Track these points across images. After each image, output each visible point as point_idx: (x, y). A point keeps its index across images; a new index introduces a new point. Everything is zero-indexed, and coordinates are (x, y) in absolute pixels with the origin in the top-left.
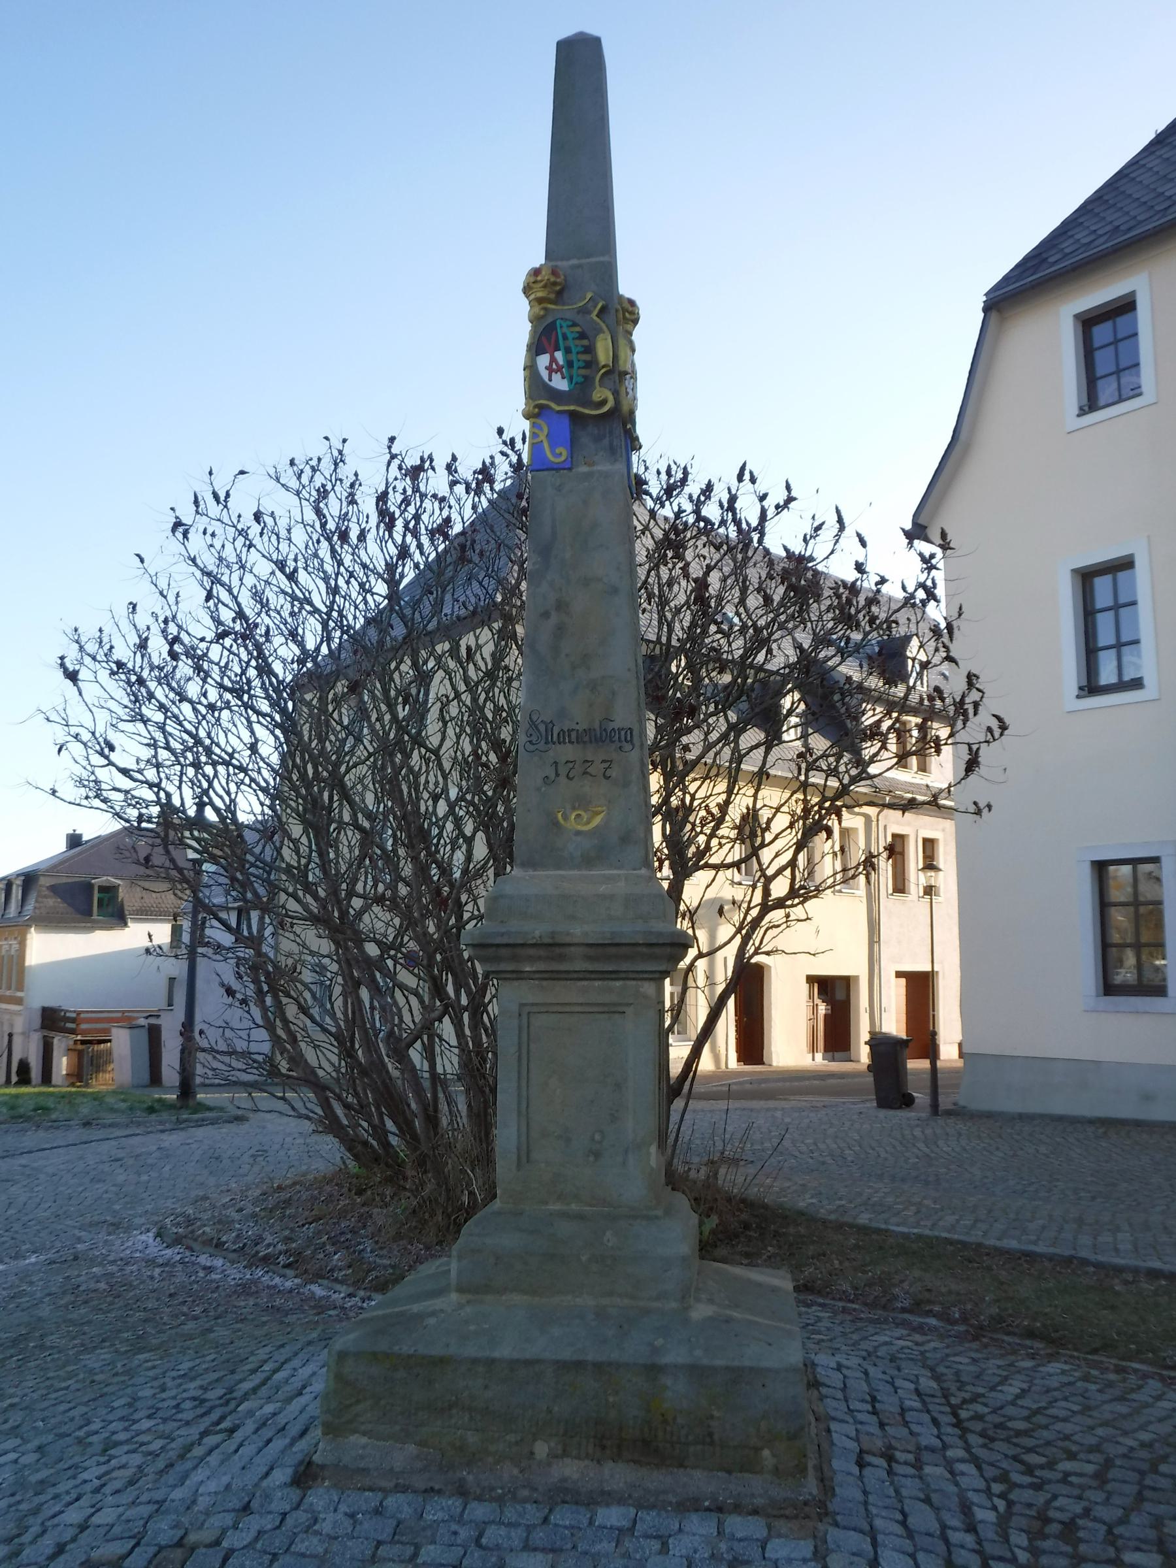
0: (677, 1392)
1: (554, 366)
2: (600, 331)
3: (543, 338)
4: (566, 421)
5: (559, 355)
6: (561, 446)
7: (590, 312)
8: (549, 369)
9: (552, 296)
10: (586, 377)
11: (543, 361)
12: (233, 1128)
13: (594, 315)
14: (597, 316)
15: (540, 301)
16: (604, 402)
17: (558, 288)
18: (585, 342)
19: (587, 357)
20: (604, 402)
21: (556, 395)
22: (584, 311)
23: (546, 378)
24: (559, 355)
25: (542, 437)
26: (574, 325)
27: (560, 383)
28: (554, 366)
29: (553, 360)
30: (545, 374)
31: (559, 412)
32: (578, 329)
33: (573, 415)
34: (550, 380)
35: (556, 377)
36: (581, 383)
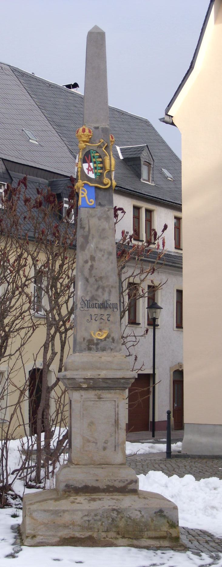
2: (106, 155)
3: (86, 157)
4: (94, 189)
5: (91, 164)
7: (102, 148)
10: (101, 173)
11: (85, 166)
13: (103, 149)
18: (101, 160)
22: (100, 147)
26: (97, 152)
27: (92, 175)
29: (89, 166)
30: (86, 171)
32: (98, 154)
35: (91, 173)
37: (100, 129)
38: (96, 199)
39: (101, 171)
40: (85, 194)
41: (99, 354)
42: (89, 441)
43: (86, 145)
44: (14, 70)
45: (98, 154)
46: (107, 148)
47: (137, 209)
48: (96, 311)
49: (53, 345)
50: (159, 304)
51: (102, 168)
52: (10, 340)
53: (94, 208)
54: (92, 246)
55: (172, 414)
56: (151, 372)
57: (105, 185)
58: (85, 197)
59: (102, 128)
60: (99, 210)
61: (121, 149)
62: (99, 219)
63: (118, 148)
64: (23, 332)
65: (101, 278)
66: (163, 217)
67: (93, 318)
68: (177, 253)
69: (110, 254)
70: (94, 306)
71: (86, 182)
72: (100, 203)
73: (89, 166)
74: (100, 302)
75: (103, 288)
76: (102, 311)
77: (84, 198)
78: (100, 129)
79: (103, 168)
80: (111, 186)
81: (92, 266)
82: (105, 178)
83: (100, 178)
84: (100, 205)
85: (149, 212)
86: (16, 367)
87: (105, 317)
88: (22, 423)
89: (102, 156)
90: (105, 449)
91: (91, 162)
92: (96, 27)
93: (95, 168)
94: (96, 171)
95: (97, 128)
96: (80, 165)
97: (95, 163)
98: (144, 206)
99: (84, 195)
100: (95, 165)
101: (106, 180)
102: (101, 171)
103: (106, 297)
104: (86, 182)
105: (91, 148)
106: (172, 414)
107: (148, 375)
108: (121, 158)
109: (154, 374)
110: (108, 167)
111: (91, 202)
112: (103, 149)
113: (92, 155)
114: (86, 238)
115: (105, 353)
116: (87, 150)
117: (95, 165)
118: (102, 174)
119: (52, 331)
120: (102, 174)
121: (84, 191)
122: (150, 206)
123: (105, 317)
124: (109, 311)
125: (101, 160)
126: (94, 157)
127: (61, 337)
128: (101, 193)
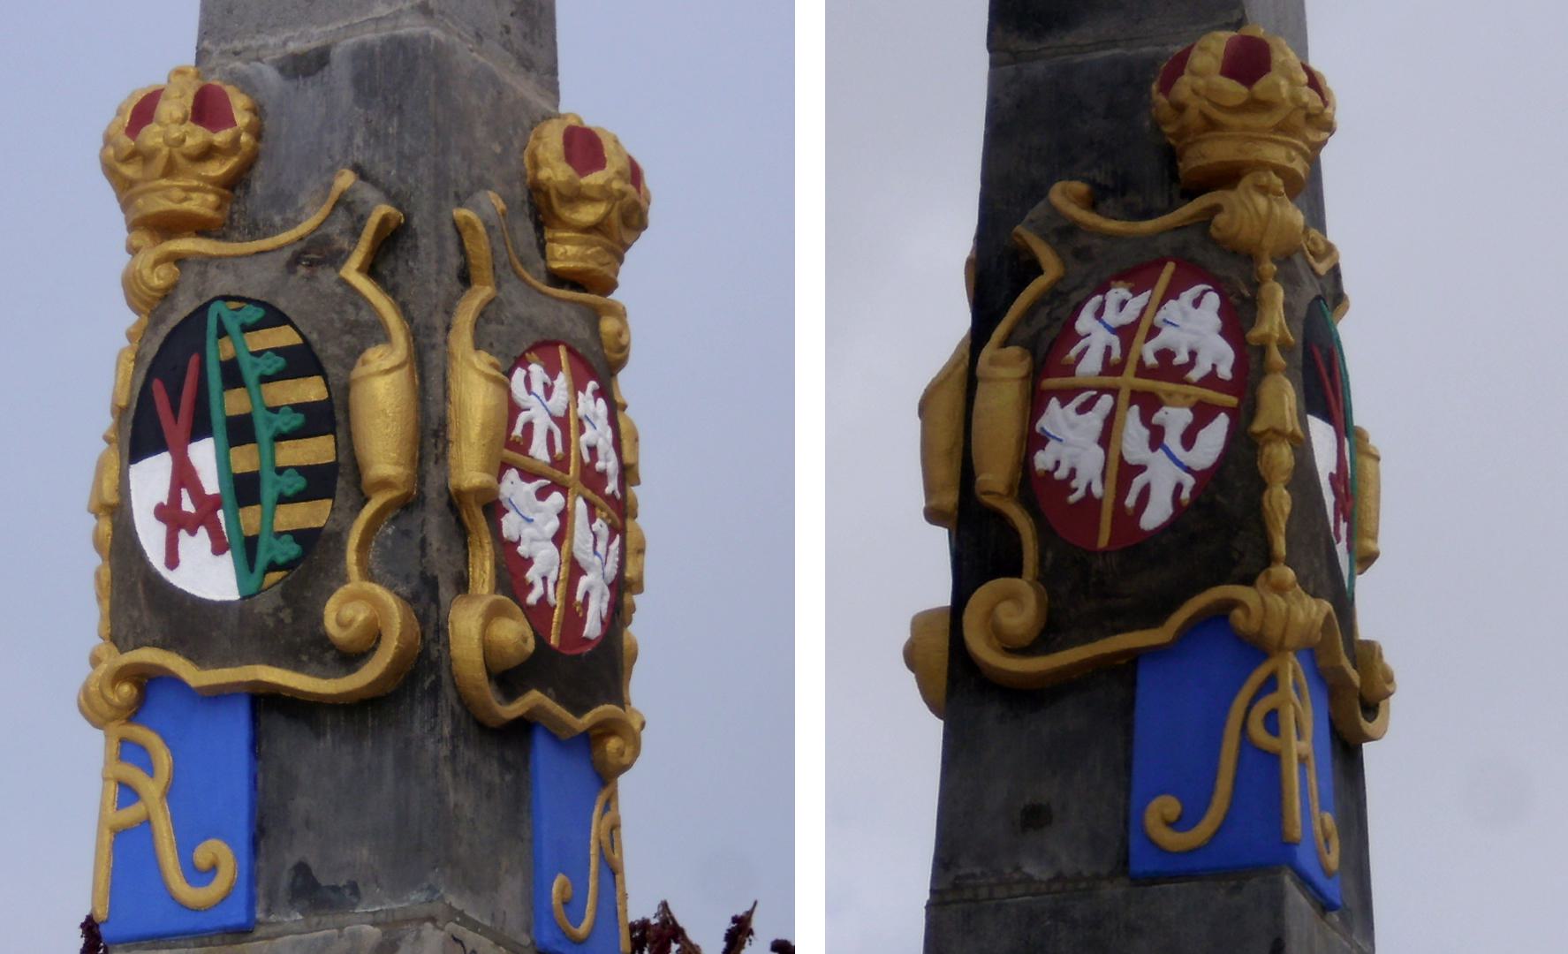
0: (513, 65)
1: (188, 505)
2: (375, 332)
3: (157, 385)
4: (235, 726)
5: (203, 454)
6: (217, 834)
7: (336, 258)
8: (169, 514)
9: (201, 204)
10: (306, 538)
11: (151, 480)
12: (622, 141)
13: (352, 272)
14: (371, 270)
15: (166, 226)
16: (374, 637)
17: (216, 169)
18: (311, 390)
19: (318, 450)
20: (374, 637)
21: (186, 622)
22: (317, 254)
23: (155, 554)
24: (203, 454)
25: (152, 789)
26: (274, 317)
27: (208, 575)
28: (188, 505)
29: (184, 476)
30: (151, 536)
31: (217, 696)
32: (284, 337)
33: (265, 702)
34: (172, 561)
35: (196, 545)
36: (289, 566)
37: (341, 70)
39: (312, 515)
43: (179, 260)
45: (284, 337)
46: (389, 251)
51: (318, 482)
53: (242, 932)
55: (1312, 763)
57: (350, 659)
58: (147, 823)
59: (363, 54)
68: (1297, 688)
71: (148, 656)
72: (302, 869)
73: (184, 476)
78: (341, 70)
80: (423, 667)
82: (356, 583)
84: (310, 892)
89: (329, 351)
91: (200, 430)
93: (245, 489)
94: (251, 518)
97: (240, 431)
100: (244, 460)
102: (312, 515)
104: (148, 656)
105: (223, 283)
106: (1312, 763)
111: (200, 875)
112: (352, 272)
113: (226, 349)
116: (185, 306)
117: (244, 460)
118: (315, 548)
121: (149, 768)
125: (311, 390)
126: (232, 375)
128: (317, 759)
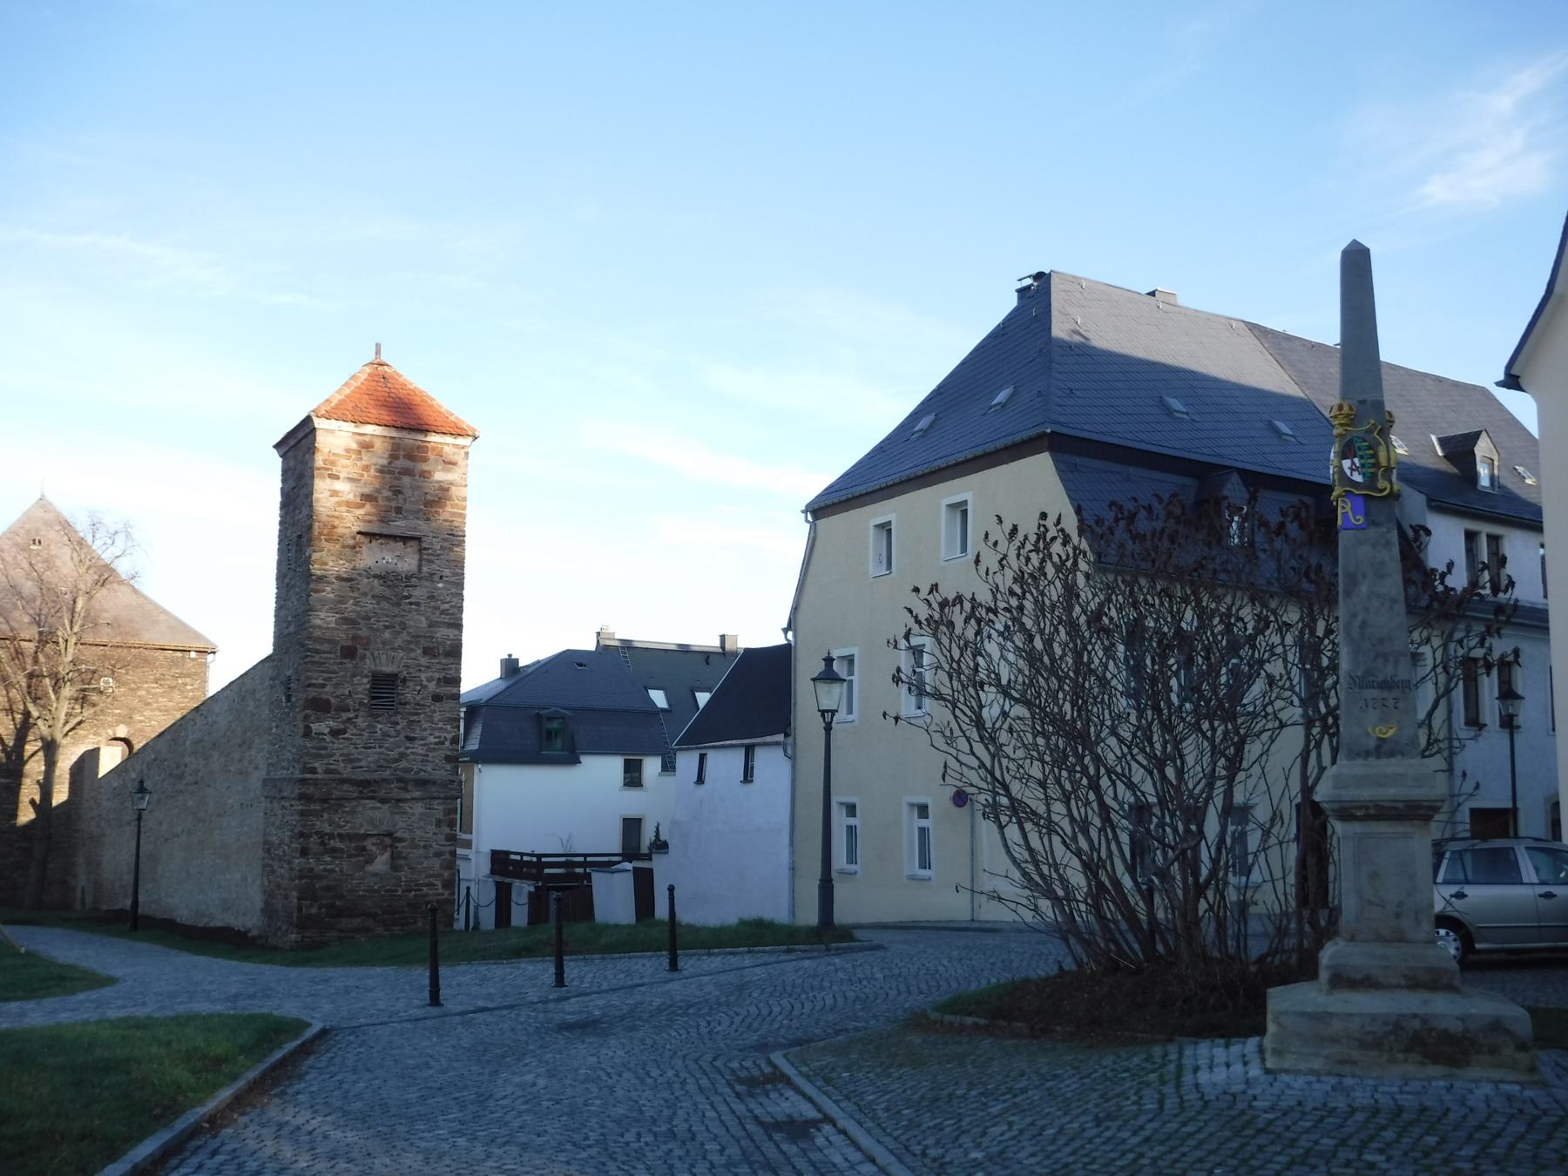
5: (1356, 460)
11: (1346, 464)
22: (1370, 431)
27: (1357, 478)
30: (1348, 472)
38: (1367, 514)
40: (1348, 508)
41: (1384, 761)
42: (1370, 903)
44: (1254, 328)
47: (1471, 536)
48: (1375, 693)
49: (1319, 756)
50: (1520, 692)
52: (1247, 747)
54: (1364, 589)
56: (1509, 805)
60: (1373, 532)
61: (1440, 440)
62: (1374, 547)
63: (1434, 438)
64: (1265, 736)
65: (1381, 641)
66: (1517, 546)
67: (1370, 704)
69: (1394, 601)
70: (1371, 686)
74: (1381, 678)
75: (1385, 656)
76: (1385, 694)
77: (1345, 514)
79: (1377, 465)
81: (1364, 623)
83: (1371, 481)
85: (1494, 540)
86: (1258, 791)
87: (1390, 703)
88: (1268, 877)
90: (1398, 916)
92: (1355, 243)
93: (1363, 466)
95: (1363, 402)
96: (1336, 462)
97: (1361, 457)
98: (1485, 529)
99: (1346, 511)
101: (1382, 483)
103: (1390, 670)
107: (1505, 811)
108: (1440, 453)
109: (1514, 811)
110: (1383, 462)
114: (1353, 580)
115: (1392, 760)
119: (1315, 731)
120: (1374, 475)
122: (1496, 530)
123: (1390, 703)
124: (1395, 693)
127: (1331, 743)
